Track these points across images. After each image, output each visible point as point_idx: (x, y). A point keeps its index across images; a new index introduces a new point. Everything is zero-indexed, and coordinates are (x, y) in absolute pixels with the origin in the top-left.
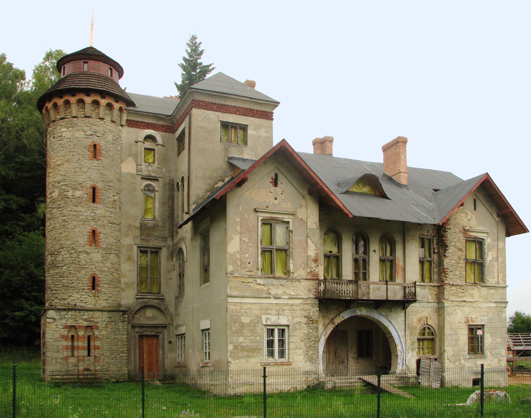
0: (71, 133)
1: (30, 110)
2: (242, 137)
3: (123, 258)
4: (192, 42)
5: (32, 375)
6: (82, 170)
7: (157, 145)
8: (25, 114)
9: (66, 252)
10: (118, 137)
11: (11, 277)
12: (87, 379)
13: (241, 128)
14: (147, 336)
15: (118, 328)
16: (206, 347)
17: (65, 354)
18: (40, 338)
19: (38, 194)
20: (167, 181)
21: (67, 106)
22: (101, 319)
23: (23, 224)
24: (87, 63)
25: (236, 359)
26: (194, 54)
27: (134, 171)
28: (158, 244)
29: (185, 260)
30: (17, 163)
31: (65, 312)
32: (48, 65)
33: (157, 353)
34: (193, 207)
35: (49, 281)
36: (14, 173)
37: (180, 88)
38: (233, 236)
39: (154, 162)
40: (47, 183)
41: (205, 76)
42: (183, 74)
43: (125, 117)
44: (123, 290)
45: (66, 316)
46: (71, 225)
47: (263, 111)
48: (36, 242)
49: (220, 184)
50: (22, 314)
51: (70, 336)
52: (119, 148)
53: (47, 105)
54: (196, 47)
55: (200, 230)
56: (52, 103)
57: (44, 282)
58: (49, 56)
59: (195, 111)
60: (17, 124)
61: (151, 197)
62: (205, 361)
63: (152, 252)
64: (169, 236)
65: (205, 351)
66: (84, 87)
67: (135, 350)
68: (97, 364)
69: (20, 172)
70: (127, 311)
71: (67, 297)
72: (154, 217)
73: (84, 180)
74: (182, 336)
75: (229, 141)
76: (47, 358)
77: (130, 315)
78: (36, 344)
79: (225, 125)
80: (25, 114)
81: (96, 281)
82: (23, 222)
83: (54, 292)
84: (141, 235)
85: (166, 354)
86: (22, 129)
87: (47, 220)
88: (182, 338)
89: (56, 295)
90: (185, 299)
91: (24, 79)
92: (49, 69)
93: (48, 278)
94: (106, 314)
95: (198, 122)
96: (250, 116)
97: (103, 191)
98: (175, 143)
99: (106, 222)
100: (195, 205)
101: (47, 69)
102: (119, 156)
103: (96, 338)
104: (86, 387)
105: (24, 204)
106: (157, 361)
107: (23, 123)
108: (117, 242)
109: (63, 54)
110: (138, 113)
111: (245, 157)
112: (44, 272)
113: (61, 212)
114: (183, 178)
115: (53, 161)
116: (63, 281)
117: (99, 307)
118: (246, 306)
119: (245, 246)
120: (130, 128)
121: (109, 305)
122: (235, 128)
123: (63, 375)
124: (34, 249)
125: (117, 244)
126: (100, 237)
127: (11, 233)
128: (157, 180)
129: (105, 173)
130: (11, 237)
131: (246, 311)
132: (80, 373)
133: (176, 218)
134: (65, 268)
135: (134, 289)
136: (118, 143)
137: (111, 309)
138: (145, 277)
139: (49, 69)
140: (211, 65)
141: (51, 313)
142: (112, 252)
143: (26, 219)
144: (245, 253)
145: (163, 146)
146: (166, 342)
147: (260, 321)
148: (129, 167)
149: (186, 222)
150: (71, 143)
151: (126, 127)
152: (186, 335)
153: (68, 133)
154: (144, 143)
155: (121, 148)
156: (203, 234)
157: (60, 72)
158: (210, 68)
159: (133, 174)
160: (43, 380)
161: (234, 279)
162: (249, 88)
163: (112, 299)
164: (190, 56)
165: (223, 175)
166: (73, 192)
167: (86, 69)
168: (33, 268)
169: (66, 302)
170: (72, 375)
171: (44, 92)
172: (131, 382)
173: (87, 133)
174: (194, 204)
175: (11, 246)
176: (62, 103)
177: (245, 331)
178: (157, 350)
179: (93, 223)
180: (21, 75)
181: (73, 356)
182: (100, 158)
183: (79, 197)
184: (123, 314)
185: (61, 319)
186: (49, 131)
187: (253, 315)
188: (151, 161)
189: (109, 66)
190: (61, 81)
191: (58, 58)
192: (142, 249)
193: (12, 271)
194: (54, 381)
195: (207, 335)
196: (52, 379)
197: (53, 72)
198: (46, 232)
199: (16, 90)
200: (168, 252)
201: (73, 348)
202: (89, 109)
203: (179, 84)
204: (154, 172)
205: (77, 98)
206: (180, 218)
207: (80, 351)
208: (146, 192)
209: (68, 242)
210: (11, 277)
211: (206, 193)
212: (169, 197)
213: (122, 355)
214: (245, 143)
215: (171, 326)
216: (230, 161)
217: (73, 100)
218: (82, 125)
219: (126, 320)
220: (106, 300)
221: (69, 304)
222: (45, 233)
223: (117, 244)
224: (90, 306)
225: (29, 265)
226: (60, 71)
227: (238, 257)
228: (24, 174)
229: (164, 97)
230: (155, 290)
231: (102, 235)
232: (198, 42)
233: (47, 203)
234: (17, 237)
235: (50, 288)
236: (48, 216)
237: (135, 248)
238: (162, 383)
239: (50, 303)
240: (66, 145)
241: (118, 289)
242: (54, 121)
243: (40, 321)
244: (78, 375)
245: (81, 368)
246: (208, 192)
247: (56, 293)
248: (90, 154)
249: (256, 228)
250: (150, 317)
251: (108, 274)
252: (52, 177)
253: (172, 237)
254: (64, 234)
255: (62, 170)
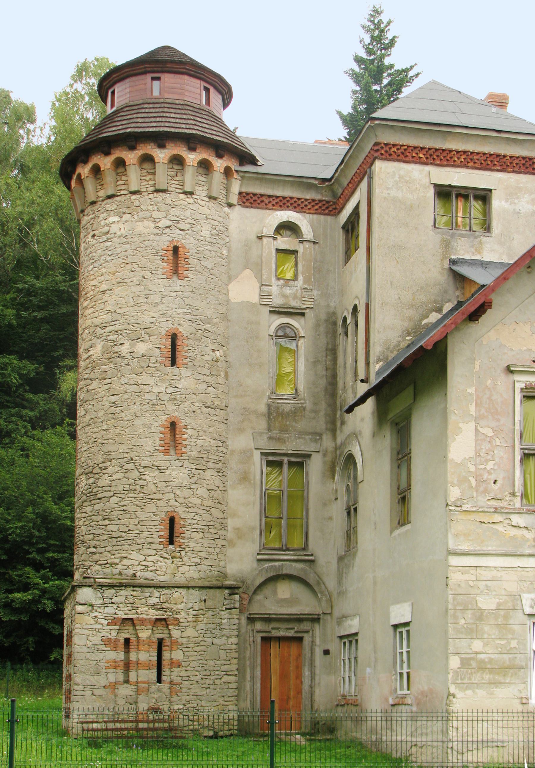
0: (127, 226)
1: (45, 183)
2: (481, 217)
3: (232, 477)
4: (373, 22)
5: (44, 723)
6: (149, 300)
7: (302, 242)
8: (35, 192)
9: (116, 469)
10: (223, 229)
11: (8, 521)
12: (154, 729)
13: (476, 198)
14: (279, 639)
15: (220, 624)
16: (402, 661)
17: (112, 678)
18: (62, 647)
19: (61, 352)
20: (323, 316)
21: (121, 170)
22: (184, 603)
23: (31, 414)
24: (158, 79)
25: (467, 688)
26: (376, 47)
27: (255, 299)
28: (303, 448)
29: (360, 479)
30: (20, 291)
31: (113, 591)
32: (80, 89)
33: (299, 676)
34: (378, 367)
35: (82, 528)
36: (14, 312)
37: (349, 121)
38: (461, 425)
39: (296, 278)
40: (80, 329)
41: (400, 92)
42: (354, 92)
43: (236, 187)
44: (231, 543)
45: (115, 600)
46: (128, 413)
47: (524, 158)
48: (57, 450)
49: (434, 317)
50: (27, 596)
51: (122, 640)
52: (225, 252)
53: (79, 170)
54: (382, 31)
55: (391, 415)
56: (90, 165)
57: (71, 530)
58: (82, 71)
59: (381, 167)
60: (21, 213)
61: (290, 351)
62: (399, 692)
63: (291, 464)
64: (327, 429)
65: (399, 671)
66: (154, 129)
67: (253, 669)
68: (174, 698)
69: (26, 310)
70: (238, 588)
71: (117, 561)
72: (297, 391)
73: (153, 320)
74: (351, 639)
75: (453, 225)
76: (76, 687)
77: (245, 596)
78: (52, 658)
79: (444, 193)
80: (37, 190)
81: (177, 527)
82: (32, 409)
83: (92, 550)
84: (269, 430)
85: (317, 678)
86: (30, 224)
87: (79, 404)
88: (351, 642)
89: (96, 557)
90: (358, 560)
91: (32, 120)
92: (82, 97)
93: (81, 523)
94: (195, 593)
95: (388, 189)
96: (498, 170)
97: (191, 342)
98: (340, 235)
99: (197, 404)
100: (381, 363)
101: (78, 97)
102: (223, 269)
103: (175, 644)
104: (152, 747)
105: (33, 375)
106: (299, 692)
107: (31, 210)
108: (220, 444)
109: (109, 65)
110: (263, 178)
111: (486, 259)
112: (73, 511)
113: (107, 387)
114: (355, 308)
115: (93, 283)
116: (110, 528)
117: (181, 579)
118: (487, 574)
119: (486, 446)
120: (248, 209)
121: (202, 574)
122: (466, 197)
123: (105, 722)
124: (53, 464)
125: (220, 449)
126: (186, 436)
127: (8, 434)
128: (303, 314)
129: (196, 304)
130: (7, 440)
131: (489, 583)
132: (141, 717)
133: (340, 392)
134: (114, 500)
135: (253, 541)
136: (222, 242)
137: (207, 584)
138: (277, 515)
139: (82, 97)
140: (412, 68)
141: (85, 594)
142: (210, 465)
143: (38, 403)
144: (487, 461)
145: (315, 243)
146: (318, 652)
147: (519, 607)
148: (244, 290)
149: (362, 400)
150: (128, 246)
151: (238, 208)
152: (360, 637)
153: (122, 226)
154: (275, 239)
155: (229, 251)
156: (397, 424)
157: (104, 100)
158: (411, 73)
159: (253, 305)
160: (65, 733)
161: (463, 517)
162: (494, 109)
163: (207, 562)
164: (370, 52)
165: (439, 299)
166: (132, 346)
167: (156, 93)
168: (49, 504)
169: (116, 571)
170: (124, 721)
171: (73, 146)
172: (244, 736)
173: (159, 225)
174: (379, 360)
175: (7, 460)
176: (109, 166)
177: (486, 628)
178: (299, 668)
179: (171, 407)
180: (25, 115)
181: (127, 681)
182: (185, 273)
183: (143, 356)
184: (230, 595)
185: (105, 605)
186: (83, 223)
187: (503, 592)
188: (289, 275)
189: (203, 84)
190: (107, 120)
191: (99, 75)
192: (271, 458)
193: (8, 509)
194: (89, 734)
195: (405, 636)
196: (83, 730)
197: (90, 104)
198: (78, 428)
199: (17, 142)
200: (325, 463)
201: (127, 666)
202: (163, 173)
203: (345, 113)
204: (295, 297)
205: (140, 151)
206: (350, 391)
207: (141, 672)
208: (280, 340)
209: (122, 448)
210: (8, 521)
211: (404, 340)
212: (327, 350)
213: (226, 678)
214: (487, 227)
215: (328, 617)
216: (454, 268)
217: (131, 157)
218: (151, 208)
219: (237, 605)
220: (197, 564)
221: (121, 574)
222: (75, 431)
223: (220, 449)
224: (164, 579)
225: (43, 498)
226: (104, 100)
227: (472, 469)
228: (35, 314)
229: (316, 142)
230: (297, 543)
231: (189, 431)
232: (385, 21)
233: (80, 371)
234: (19, 442)
235: (83, 542)
236: (81, 395)
237: (257, 455)
238: (307, 740)
239: (84, 573)
240: (118, 251)
241: (220, 543)
242: (93, 203)
243: (62, 611)
244: (137, 721)
245: (143, 706)
246: (409, 334)
247: (95, 553)
248: (165, 267)
249: (511, 408)
250: (285, 599)
251: (201, 512)
252: (91, 317)
253: (333, 431)
254: (113, 432)
255: (111, 301)
